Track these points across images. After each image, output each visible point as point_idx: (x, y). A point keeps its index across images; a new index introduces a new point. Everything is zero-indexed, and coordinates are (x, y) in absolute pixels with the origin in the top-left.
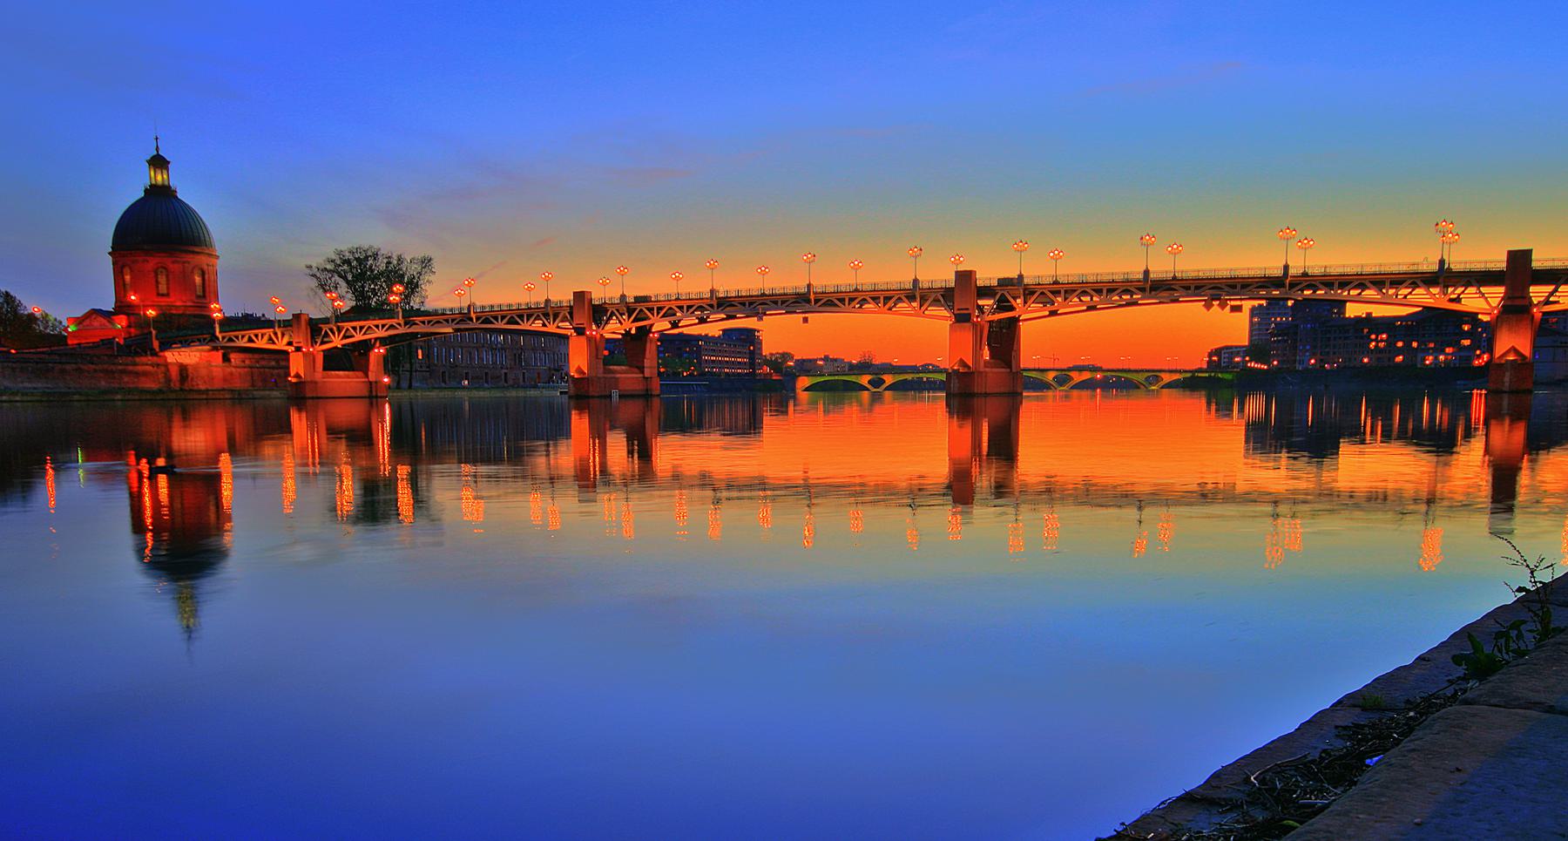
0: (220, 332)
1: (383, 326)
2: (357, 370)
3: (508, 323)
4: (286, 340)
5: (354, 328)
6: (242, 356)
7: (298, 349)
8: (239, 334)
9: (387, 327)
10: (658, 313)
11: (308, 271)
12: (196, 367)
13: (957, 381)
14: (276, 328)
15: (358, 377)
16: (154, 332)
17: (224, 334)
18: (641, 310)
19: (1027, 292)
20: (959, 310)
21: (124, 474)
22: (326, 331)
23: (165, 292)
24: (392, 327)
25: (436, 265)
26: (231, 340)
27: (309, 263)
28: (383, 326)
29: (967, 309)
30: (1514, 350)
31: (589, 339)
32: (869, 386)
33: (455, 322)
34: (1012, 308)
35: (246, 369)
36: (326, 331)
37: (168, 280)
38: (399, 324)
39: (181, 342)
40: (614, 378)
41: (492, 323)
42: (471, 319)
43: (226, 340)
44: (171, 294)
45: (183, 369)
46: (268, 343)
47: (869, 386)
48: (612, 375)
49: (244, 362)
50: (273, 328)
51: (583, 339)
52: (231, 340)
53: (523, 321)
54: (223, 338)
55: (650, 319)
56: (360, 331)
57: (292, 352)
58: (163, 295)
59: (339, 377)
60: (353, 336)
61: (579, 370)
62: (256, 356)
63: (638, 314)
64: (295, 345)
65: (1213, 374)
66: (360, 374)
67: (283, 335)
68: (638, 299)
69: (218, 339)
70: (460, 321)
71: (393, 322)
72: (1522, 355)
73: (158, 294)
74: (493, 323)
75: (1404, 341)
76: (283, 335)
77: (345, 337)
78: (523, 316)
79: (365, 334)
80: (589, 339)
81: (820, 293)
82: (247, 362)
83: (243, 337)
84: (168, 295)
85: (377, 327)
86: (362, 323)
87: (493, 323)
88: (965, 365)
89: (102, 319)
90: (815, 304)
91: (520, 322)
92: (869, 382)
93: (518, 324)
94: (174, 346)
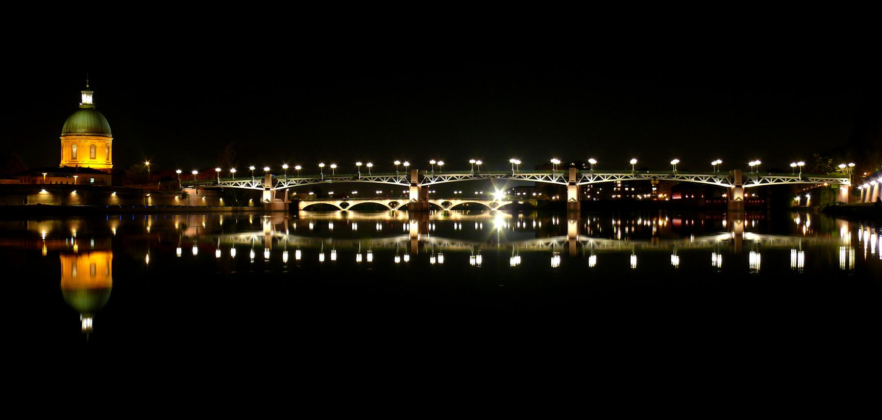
3: (234, 185)
4: (257, 185)
8: (242, 181)
21: (432, 227)
23: (94, 157)
24: (626, 177)
26: (225, 184)
30: (739, 198)
32: (340, 207)
33: (623, 177)
37: (95, 151)
41: (239, 186)
43: (233, 184)
47: (340, 207)
51: (269, 192)
53: (553, 179)
54: (220, 184)
60: (283, 186)
61: (267, 200)
65: (753, 201)
69: (218, 184)
72: (574, 200)
73: (91, 158)
74: (537, 179)
75: (591, 196)
84: (95, 158)
86: (529, 174)
88: (415, 200)
91: (394, 180)
92: (389, 204)
93: (394, 182)
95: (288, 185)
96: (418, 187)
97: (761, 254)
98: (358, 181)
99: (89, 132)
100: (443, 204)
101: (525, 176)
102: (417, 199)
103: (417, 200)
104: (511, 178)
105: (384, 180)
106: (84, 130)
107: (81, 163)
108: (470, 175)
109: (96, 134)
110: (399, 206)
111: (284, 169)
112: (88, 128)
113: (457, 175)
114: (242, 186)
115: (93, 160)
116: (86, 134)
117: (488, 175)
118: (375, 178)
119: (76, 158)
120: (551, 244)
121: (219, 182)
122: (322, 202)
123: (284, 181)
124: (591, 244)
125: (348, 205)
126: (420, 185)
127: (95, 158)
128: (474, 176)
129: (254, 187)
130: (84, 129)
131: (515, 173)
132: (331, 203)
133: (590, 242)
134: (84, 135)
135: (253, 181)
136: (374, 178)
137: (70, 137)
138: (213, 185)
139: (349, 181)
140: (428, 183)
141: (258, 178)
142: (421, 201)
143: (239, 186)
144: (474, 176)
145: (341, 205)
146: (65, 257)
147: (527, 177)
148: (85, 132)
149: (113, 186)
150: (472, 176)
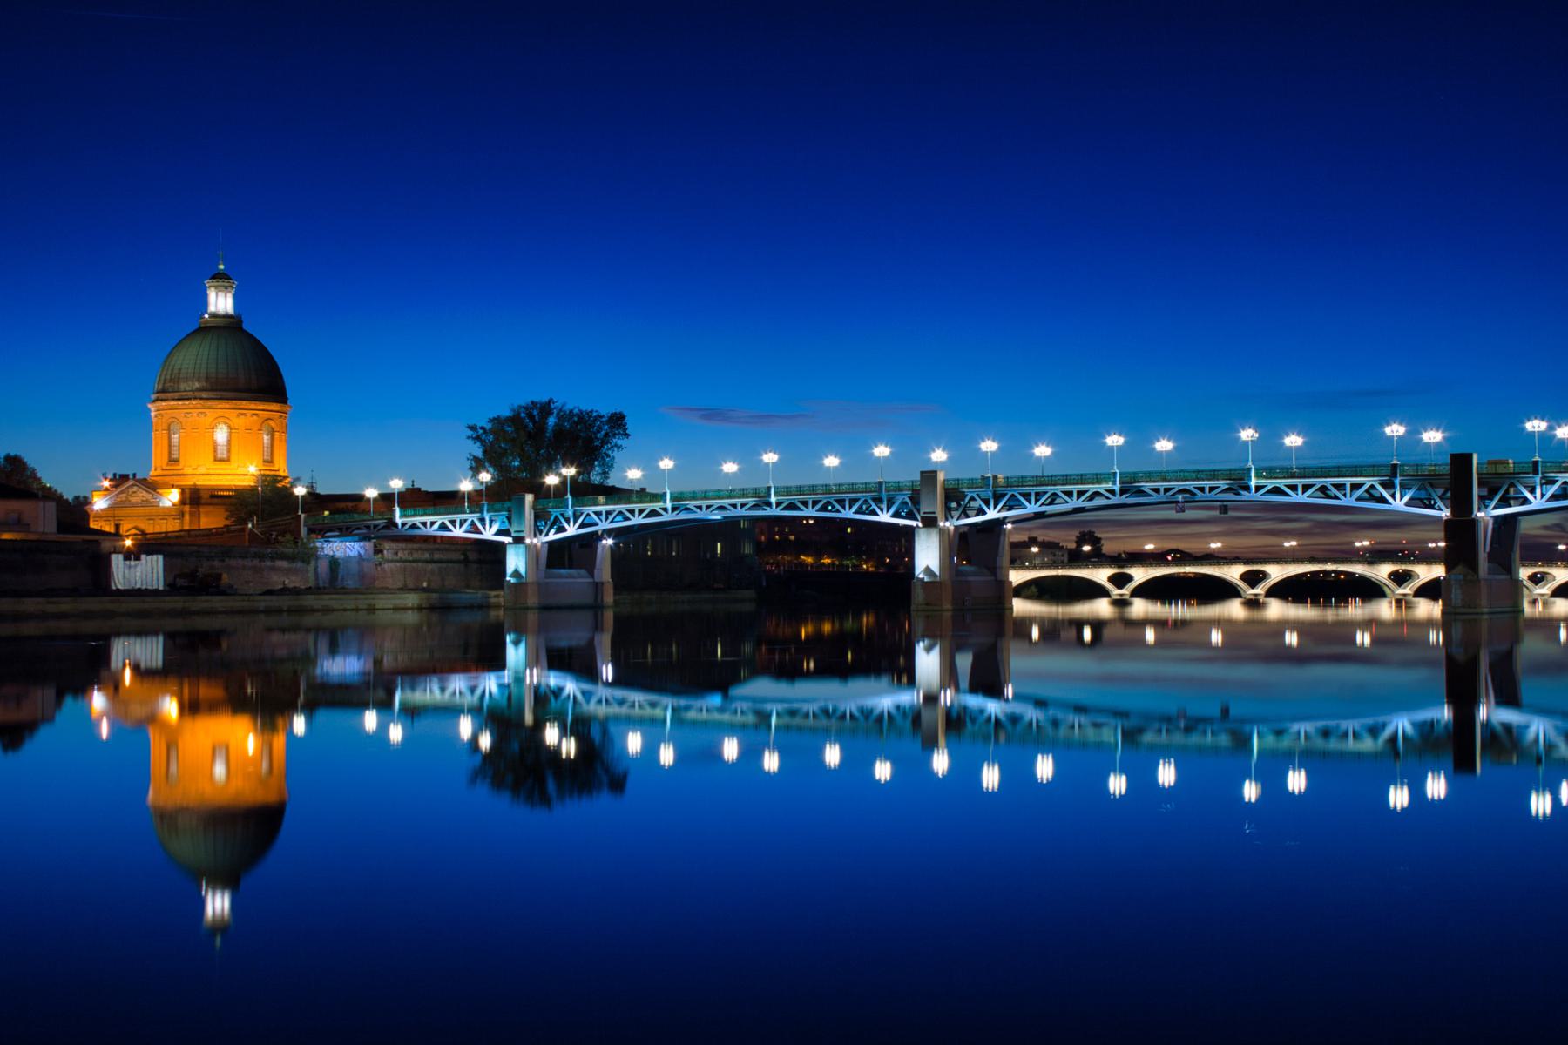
0: (401, 516)
1: (641, 511)
2: (581, 568)
4: (495, 527)
5: (598, 514)
6: (394, 546)
7: (519, 540)
8: (428, 519)
9: (784, 505)
10: (607, 518)
11: (470, 433)
12: (348, 559)
13: (1459, 592)
14: (485, 512)
15: (582, 577)
16: (303, 516)
17: (405, 520)
18: (588, 515)
19: (1543, 481)
20: (925, 513)
22: (556, 517)
23: (225, 456)
25: (630, 423)
26: (791, 506)
27: (472, 423)
28: (641, 511)
29: (934, 513)
31: (528, 547)
32: (1241, 584)
34: (1525, 501)
35: (398, 564)
36: (556, 517)
38: (665, 510)
39: (340, 529)
40: (966, 581)
42: (769, 504)
44: (232, 458)
45: (334, 562)
46: (467, 532)
48: (964, 578)
49: (397, 554)
50: (481, 511)
51: (521, 548)
52: (443, 527)
53: (455, 527)
55: (1026, 508)
56: (461, 525)
57: (510, 543)
58: (221, 460)
59: (561, 576)
60: (596, 524)
61: (928, 570)
62: (410, 546)
63: (585, 519)
64: (513, 534)
66: (583, 572)
67: (491, 521)
68: (1009, 483)
70: (754, 506)
71: (657, 506)
73: (216, 459)
76: (491, 521)
77: (582, 526)
78: (1030, 494)
79: (612, 521)
80: (528, 547)
81: (1485, 474)
82: (400, 554)
83: (433, 523)
84: (228, 460)
85: (453, 522)
87: (801, 510)
89: (144, 493)
90: (1256, 491)
94: (328, 534)
95: (580, 527)
96: (942, 532)
97: (840, 745)
98: (769, 512)
99: (212, 390)
100: (1244, 577)
101: (1294, 488)
102: (936, 570)
103: (937, 571)
104: (1245, 495)
105: (807, 507)
106: (197, 385)
107: (190, 472)
108: (1109, 486)
109: (245, 395)
110: (1417, 583)
111: (549, 486)
112: (207, 379)
113: (1200, 483)
114: (458, 532)
115: (223, 465)
116: (204, 395)
117: (1166, 484)
118: (644, 510)
119: (176, 461)
120: (1388, 732)
121: (1253, 483)
122: (1061, 572)
123: (983, 495)
124: (569, 696)
125: (1129, 578)
126: (948, 525)
127: (228, 460)
128: (1123, 492)
129: (489, 534)
130: (199, 381)
131: (1258, 477)
132: (1358, 569)
133: (599, 694)
134: (195, 398)
135: (487, 516)
136: (1080, 493)
137: (164, 404)
138: (756, 507)
139: (744, 512)
140: (977, 515)
141: (499, 506)
142: (959, 573)
143: (877, 515)
144: (1123, 492)
145: (1112, 579)
146: (577, 681)
147: (704, 508)
148: (199, 390)
149: (62, 537)
150: (1117, 487)
